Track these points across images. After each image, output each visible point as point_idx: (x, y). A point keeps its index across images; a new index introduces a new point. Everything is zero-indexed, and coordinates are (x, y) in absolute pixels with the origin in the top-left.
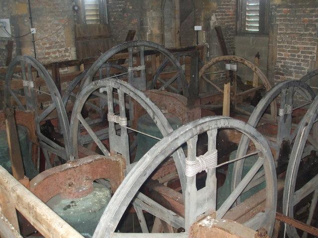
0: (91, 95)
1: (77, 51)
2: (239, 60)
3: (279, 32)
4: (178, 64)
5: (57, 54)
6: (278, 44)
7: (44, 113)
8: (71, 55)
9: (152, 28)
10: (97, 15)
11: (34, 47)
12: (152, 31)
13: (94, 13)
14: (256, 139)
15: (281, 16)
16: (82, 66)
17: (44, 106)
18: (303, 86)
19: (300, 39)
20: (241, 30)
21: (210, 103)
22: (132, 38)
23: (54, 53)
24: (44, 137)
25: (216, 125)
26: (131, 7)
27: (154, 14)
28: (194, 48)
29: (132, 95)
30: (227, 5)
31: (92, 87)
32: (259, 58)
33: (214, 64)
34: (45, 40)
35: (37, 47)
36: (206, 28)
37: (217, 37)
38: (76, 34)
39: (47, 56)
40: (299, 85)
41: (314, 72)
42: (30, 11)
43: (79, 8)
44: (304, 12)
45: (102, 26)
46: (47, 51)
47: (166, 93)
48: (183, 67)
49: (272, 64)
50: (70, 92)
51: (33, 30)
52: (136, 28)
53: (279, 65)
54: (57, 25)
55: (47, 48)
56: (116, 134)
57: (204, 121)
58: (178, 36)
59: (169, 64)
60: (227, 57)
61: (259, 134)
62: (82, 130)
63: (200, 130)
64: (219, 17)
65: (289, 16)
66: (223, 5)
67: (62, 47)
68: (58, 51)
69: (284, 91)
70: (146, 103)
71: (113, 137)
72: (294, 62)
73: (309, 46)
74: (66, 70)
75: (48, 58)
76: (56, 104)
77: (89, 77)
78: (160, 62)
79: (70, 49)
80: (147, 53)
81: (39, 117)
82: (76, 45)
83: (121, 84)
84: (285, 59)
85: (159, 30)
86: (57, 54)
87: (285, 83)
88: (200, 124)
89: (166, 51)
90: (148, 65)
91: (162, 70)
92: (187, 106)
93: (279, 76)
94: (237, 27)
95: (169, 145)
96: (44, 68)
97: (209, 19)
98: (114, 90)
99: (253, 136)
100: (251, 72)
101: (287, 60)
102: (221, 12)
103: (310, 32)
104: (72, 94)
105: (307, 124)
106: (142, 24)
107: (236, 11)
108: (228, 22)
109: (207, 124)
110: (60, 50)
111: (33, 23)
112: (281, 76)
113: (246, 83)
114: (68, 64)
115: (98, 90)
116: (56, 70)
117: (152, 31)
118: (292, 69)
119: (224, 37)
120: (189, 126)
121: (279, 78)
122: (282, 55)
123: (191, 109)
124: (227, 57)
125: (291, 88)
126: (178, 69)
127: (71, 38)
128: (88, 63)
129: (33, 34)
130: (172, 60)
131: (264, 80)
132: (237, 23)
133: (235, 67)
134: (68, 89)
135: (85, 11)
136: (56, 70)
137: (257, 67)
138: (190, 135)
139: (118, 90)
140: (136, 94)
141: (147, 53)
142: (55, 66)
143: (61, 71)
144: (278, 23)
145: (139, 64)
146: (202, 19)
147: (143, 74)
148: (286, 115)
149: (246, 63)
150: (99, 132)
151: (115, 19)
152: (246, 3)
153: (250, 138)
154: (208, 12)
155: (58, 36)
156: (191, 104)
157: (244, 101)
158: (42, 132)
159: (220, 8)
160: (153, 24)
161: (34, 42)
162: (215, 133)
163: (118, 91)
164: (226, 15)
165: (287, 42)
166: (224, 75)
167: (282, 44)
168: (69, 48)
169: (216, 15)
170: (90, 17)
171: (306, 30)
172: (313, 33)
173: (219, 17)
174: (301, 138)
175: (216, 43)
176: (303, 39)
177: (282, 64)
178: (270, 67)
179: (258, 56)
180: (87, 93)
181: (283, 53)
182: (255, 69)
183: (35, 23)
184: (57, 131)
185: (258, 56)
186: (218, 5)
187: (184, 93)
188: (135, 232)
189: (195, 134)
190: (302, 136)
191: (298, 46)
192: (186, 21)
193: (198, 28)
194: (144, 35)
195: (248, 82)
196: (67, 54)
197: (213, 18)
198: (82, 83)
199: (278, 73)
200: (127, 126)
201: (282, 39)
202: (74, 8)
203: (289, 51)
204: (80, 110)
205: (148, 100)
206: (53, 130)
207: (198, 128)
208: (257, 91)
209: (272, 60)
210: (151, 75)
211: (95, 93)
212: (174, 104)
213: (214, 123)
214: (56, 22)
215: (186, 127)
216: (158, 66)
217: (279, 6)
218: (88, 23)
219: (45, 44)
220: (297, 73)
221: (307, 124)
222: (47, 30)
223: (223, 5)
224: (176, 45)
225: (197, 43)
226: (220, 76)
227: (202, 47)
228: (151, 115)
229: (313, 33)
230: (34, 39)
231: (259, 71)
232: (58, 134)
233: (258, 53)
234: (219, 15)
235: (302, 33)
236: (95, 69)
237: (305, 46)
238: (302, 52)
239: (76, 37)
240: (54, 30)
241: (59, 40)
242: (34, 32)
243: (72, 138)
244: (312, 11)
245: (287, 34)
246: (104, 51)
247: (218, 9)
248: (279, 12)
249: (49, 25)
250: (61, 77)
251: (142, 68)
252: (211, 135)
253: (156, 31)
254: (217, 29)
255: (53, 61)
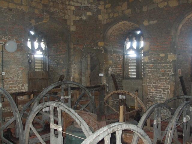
0: (38, 113)
1: (29, 87)
2: (127, 93)
3: (148, 77)
4: (91, 95)
5: (17, 88)
6: (148, 84)
7: (7, 124)
8: (25, 89)
9: (75, 75)
10: (41, 66)
11: (3, 84)
12: (74, 76)
13: (40, 65)
14: (144, 137)
15: (149, 68)
16: (32, 96)
17: (6, 120)
18: (166, 107)
19: (160, 81)
20: (126, 76)
21: (109, 119)
22: (62, 80)
23: (15, 87)
24: (5, 139)
25: (122, 127)
26: (62, 62)
27: (76, 66)
28: (99, 86)
29: (66, 111)
30: (118, 62)
31: (41, 106)
32: (138, 92)
33: (112, 95)
34: (10, 79)
35: (4, 83)
36: (106, 75)
37: (112, 80)
38: (29, 76)
39: (10, 89)
40: (164, 106)
41: (170, 99)
42: (2, 62)
43: (32, 61)
44: (161, 66)
45: (44, 73)
46: (10, 86)
47: (84, 112)
48: (93, 97)
49: (145, 95)
50: (24, 111)
51: (3, 73)
52: (65, 74)
53: (149, 96)
54: (18, 70)
55: (11, 84)
56: (55, 137)
57: (114, 125)
58: (89, 79)
59: (85, 95)
60: (119, 91)
61: (146, 134)
62: (32, 135)
63: (113, 131)
64: (113, 69)
65: (153, 68)
66: (115, 62)
67: (20, 84)
68: (18, 86)
69: (156, 109)
70: (75, 116)
71: (53, 139)
72: (158, 94)
73: (165, 85)
74: (21, 98)
75: (11, 90)
76: (16, 118)
77: (37, 101)
78: (80, 94)
79: (25, 85)
80: (72, 89)
81: (3, 126)
82: (29, 83)
83: (60, 105)
84: (152, 92)
85: (78, 75)
86: (17, 88)
87: (156, 104)
88: (112, 127)
89: (84, 87)
90: (72, 96)
91: (80, 98)
92: (97, 120)
93: (150, 102)
94: (123, 74)
95: (94, 140)
96: (10, 95)
97: (108, 70)
98: (55, 109)
99: (142, 135)
100: (133, 100)
101: (154, 93)
102: (114, 66)
103: (166, 77)
104: (25, 112)
105: (171, 129)
106: (68, 72)
107: (123, 66)
108: (119, 72)
109: (116, 127)
110: (19, 85)
111: (4, 68)
112: (151, 103)
113: (130, 107)
114: (23, 94)
115: (42, 110)
116: (16, 98)
117: (74, 76)
118: (157, 99)
119: (116, 80)
120: (106, 128)
121: (150, 104)
122: (151, 90)
123: (100, 121)
124: (119, 91)
125: (160, 108)
126: (90, 98)
127: (26, 79)
128: (36, 94)
129: (3, 75)
130: (87, 92)
131: (142, 105)
132: (123, 73)
133: (124, 97)
134: (23, 109)
135: (35, 63)
136: (16, 98)
137: (137, 97)
138: (106, 133)
139: (58, 108)
140: (69, 111)
141: (72, 89)
142: (15, 95)
143: (19, 98)
144: (147, 72)
145: (68, 95)
146: (104, 70)
147: (69, 101)
148: (157, 124)
149: (131, 94)
150: (44, 136)
151: (52, 68)
152: (128, 61)
153: (140, 135)
154: (107, 66)
155: (18, 77)
156: (99, 119)
157: (130, 117)
158: (4, 136)
159: (114, 64)
160: (75, 72)
161: (3, 80)
162: (121, 132)
163: (58, 109)
164: (117, 68)
165: (153, 83)
166: (117, 102)
167: (150, 84)
168: (24, 84)
169: (112, 68)
170: (38, 67)
171: (163, 76)
172: (168, 78)
173: (113, 69)
174: (169, 137)
175: (112, 84)
176: (162, 81)
177: (151, 95)
178: (144, 97)
179: (137, 91)
180: (37, 110)
181: (151, 89)
182: (136, 98)
183: (5, 69)
184: (14, 136)
185: (137, 91)
186: (113, 62)
187: (94, 112)
188: (116, 140)
189: (109, 133)
190: (169, 136)
191: (160, 85)
192: (94, 71)
193: (101, 75)
194: (70, 78)
195: (131, 106)
196: (23, 88)
197: (110, 69)
198: (32, 106)
199: (149, 101)
200: (63, 131)
201: (150, 81)
202: (29, 61)
203: (155, 88)
204: (31, 121)
205: (76, 114)
206: (11, 135)
207: (111, 129)
208: (137, 112)
209: (145, 93)
210: (73, 102)
211: (41, 112)
212: (89, 119)
213: (120, 126)
214: (18, 69)
215: (104, 128)
216: (78, 97)
217: (147, 63)
218: (36, 70)
219: (10, 81)
220: (160, 100)
221: (171, 129)
222: (12, 73)
223: (115, 62)
224: (88, 85)
225: (101, 84)
226: (114, 103)
227: (104, 86)
228: (79, 123)
229: (168, 78)
230: (3, 78)
231: (138, 99)
232: (15, 138)
233: (137, 89)
234: (113, 68)
235: (161, 78)
236: (41, 97)
237: (164, 85)
238: (162, 89)
239: (29, 78)
240: (16, 73)
241: (18, 80)
242: (4, 74)
243: (25, 140)
244: (166, 66)
245: (153, 78)
246: (45, 87)
247: (113, 64)
248: (147, 66)
249: (13, 70)
250: (18, 101)
251: (69, 97)
252: (119, 134)
253: (77, 76)
254: (112, 75)
255: (14, 92)
